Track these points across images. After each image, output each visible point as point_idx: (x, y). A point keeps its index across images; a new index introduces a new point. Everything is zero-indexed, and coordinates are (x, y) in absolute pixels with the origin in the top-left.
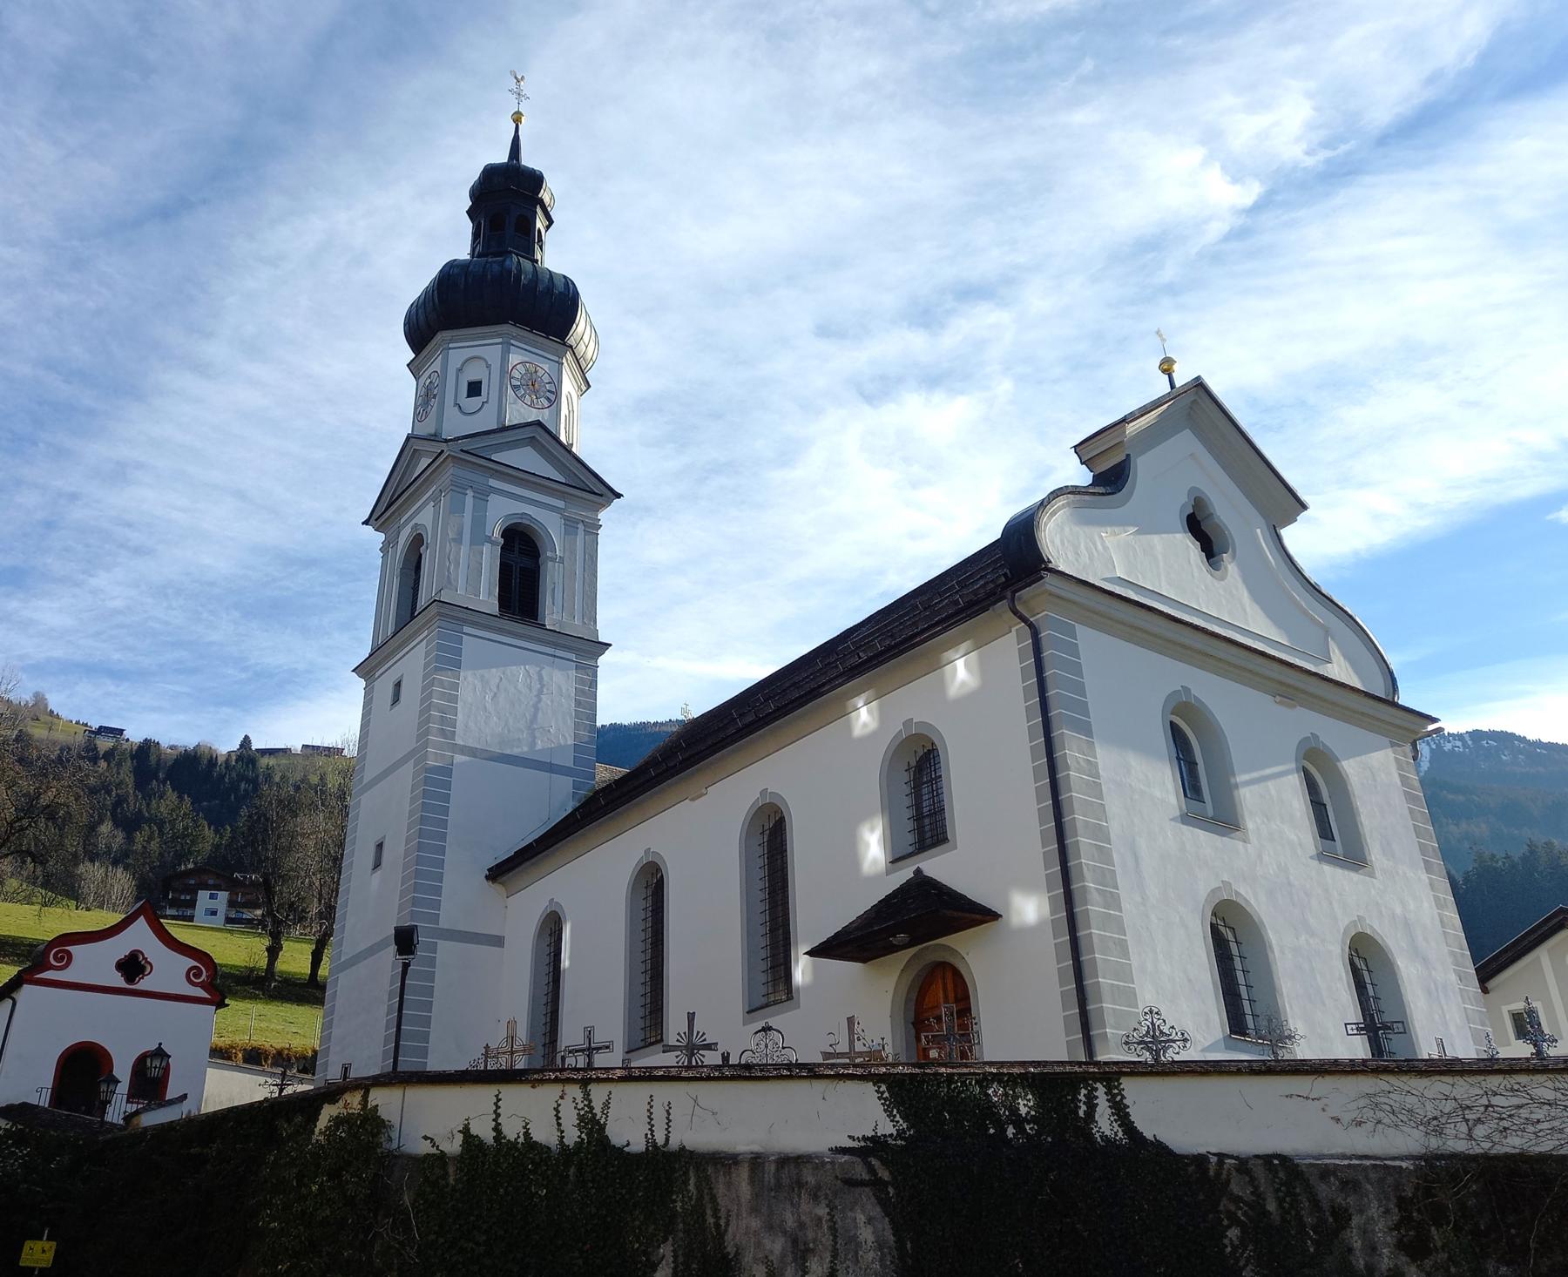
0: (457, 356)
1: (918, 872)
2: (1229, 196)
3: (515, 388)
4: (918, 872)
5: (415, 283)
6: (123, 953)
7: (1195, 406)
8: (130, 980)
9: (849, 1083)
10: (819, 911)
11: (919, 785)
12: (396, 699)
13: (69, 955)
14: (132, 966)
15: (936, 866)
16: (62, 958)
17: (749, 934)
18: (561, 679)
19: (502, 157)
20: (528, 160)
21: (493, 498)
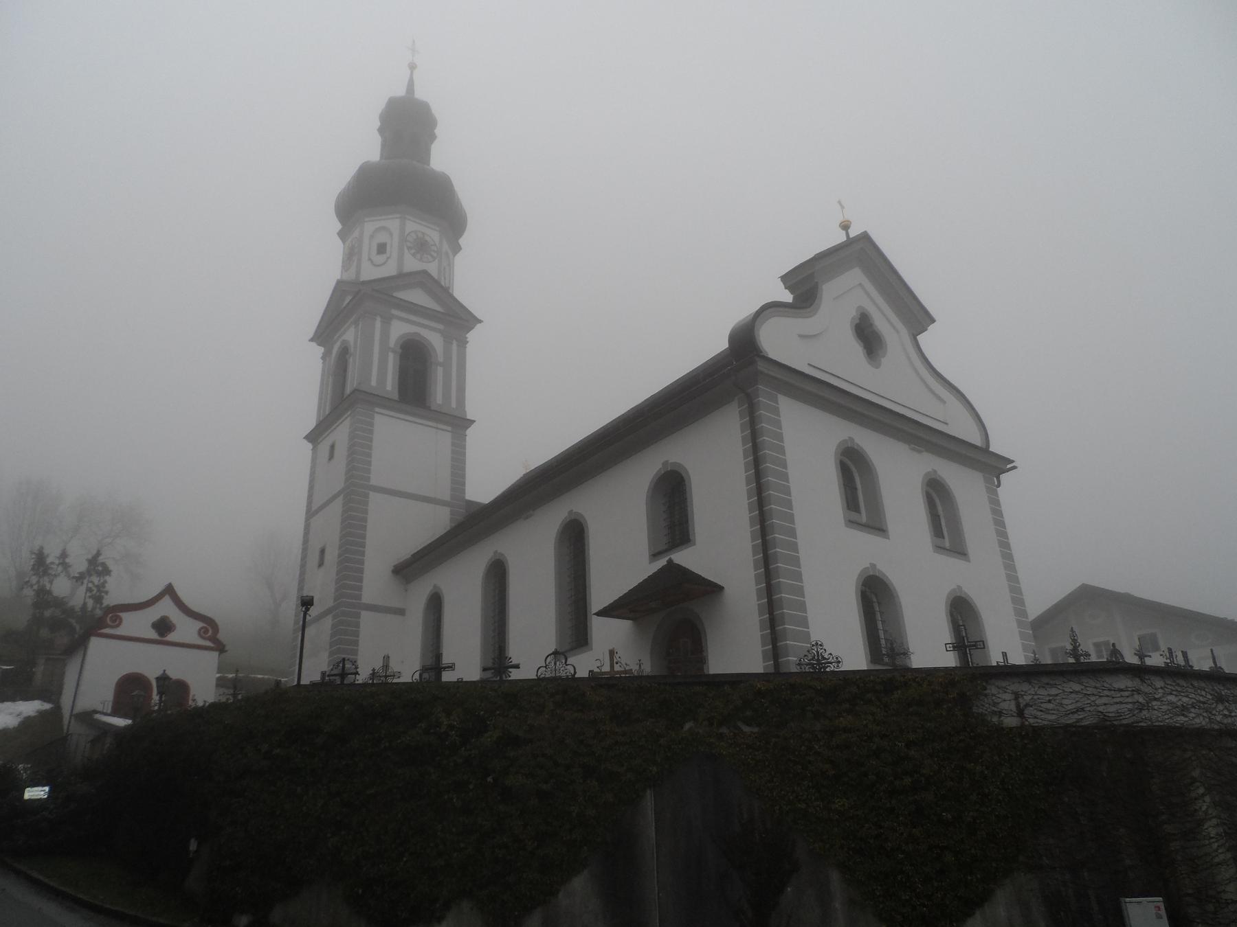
0: (369, 227)
1: (670, 561)
2: (1206, 666)
3: (409, 248)
4: (670, 561)
5: (341, 176)
7: (860, 253)
8: (162, 634)
10: (603, 591)
12: (331, 457)
13: (121, 620)
14: (163, 626)
15: (683, 558)
18: (442, 438)
19: (400, 92)
20: (420, 94)
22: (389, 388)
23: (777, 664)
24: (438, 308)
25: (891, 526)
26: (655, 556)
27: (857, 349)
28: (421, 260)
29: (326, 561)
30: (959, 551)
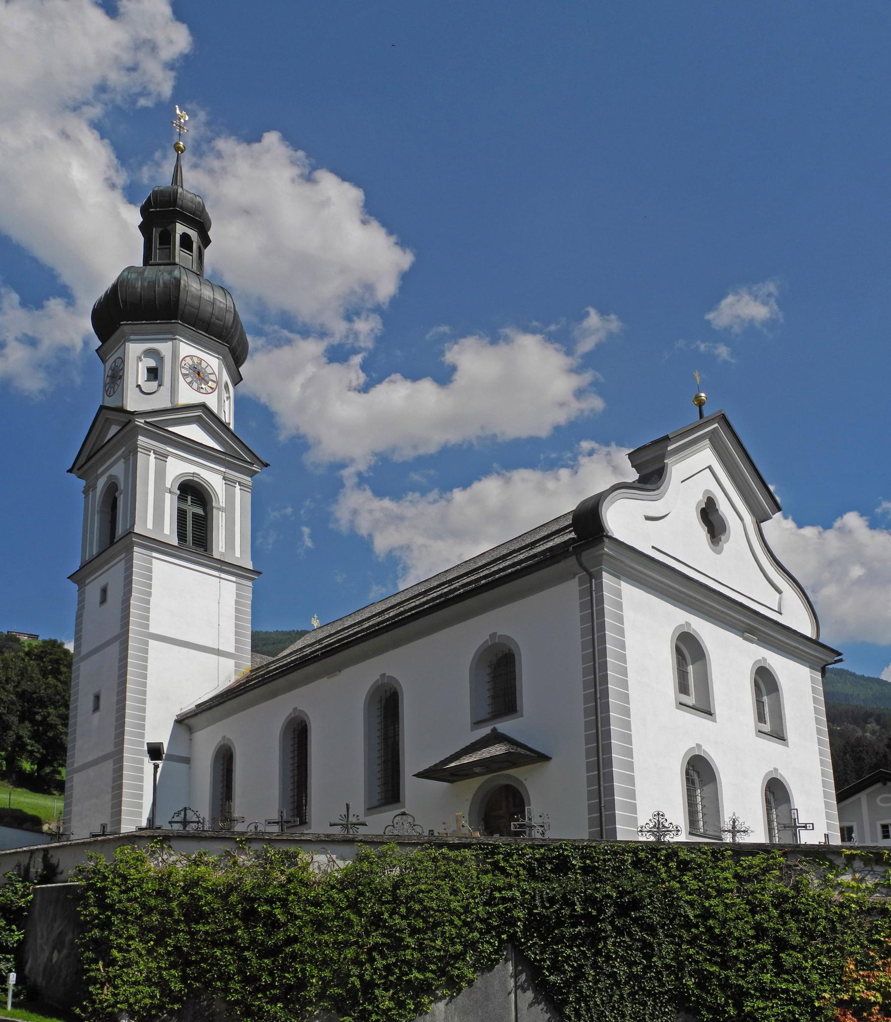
0: (134, 349)
1: (494, 730)
4: (494, 730)
11: (500, 680)
12: (103, 600)
21: (170, 459)
22: (167, 531)
23: (277, 823)
25: (719, 708)
26: (477, 723)
27: (701, 532)
28: (198, 390)
29: (101, 707)
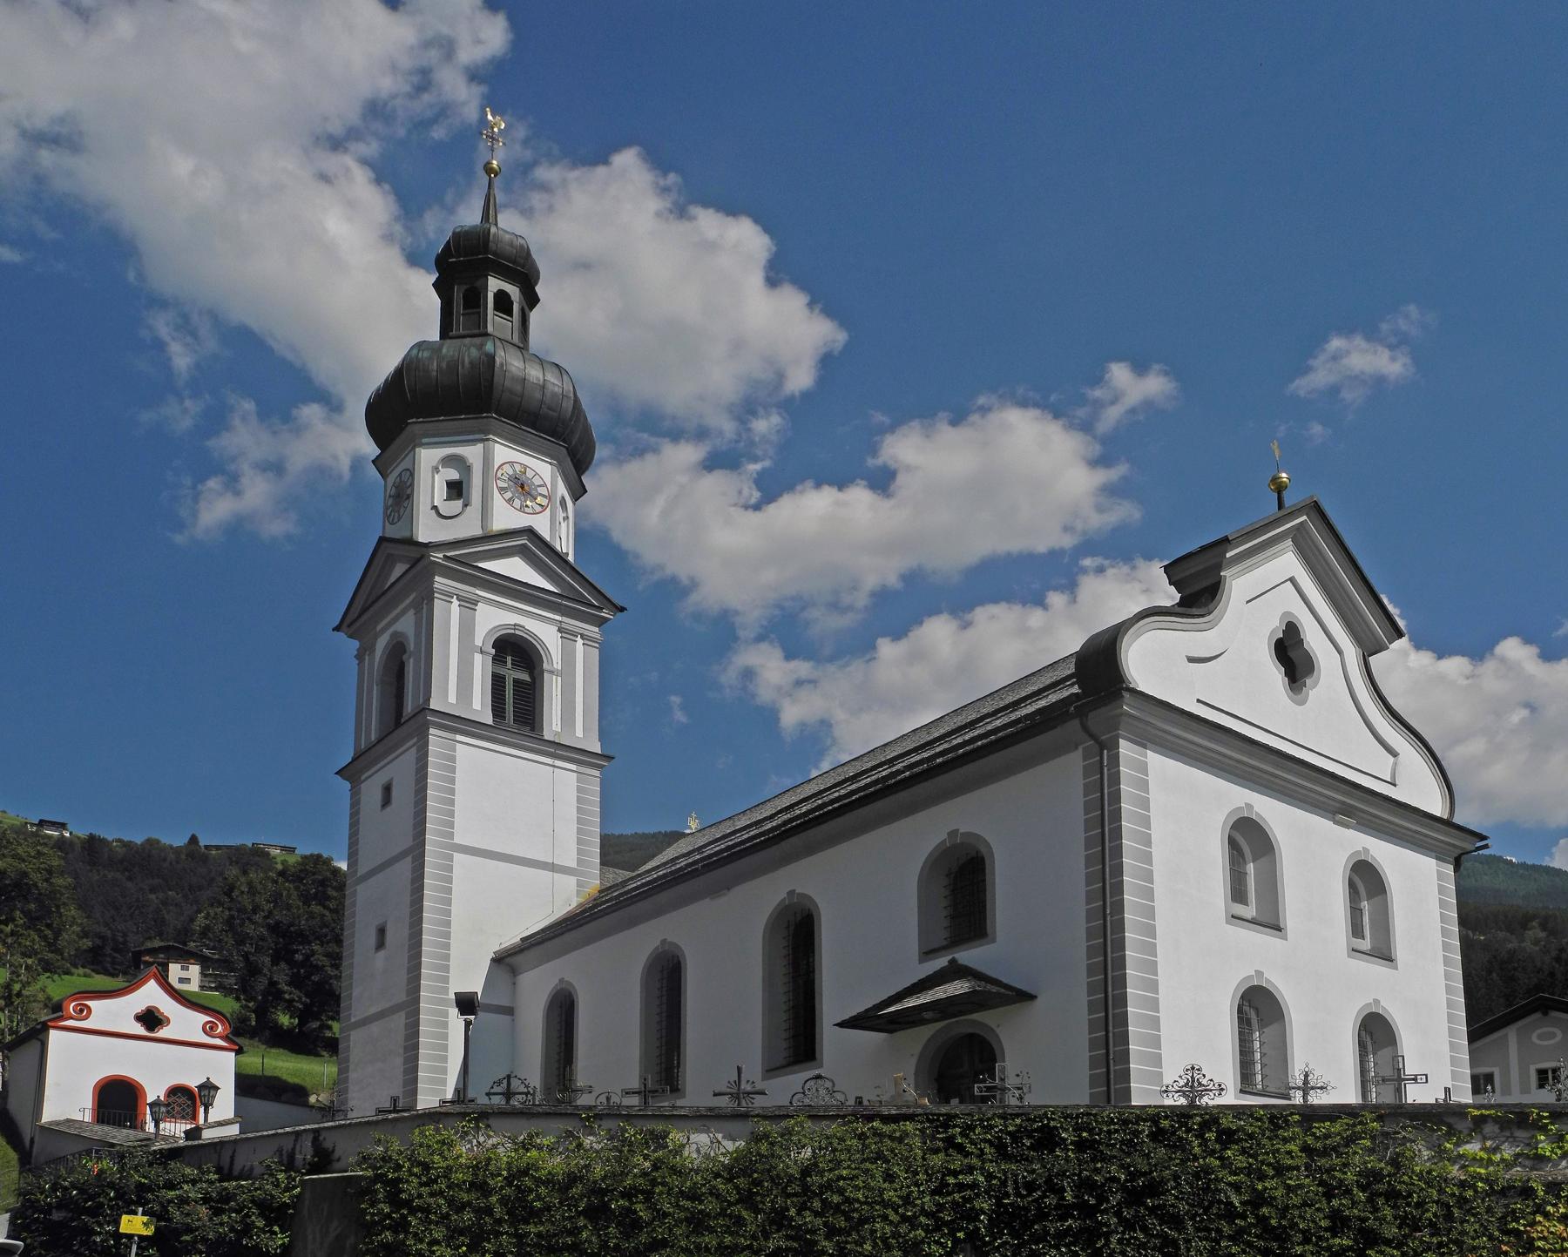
3: (501, 489)
6: (140, 1008)
8: (150, 1028)
9: (1005, 981)
10: (838, 998)
11: (962, 889)
13: (89, 1008)
16: (81, 1011)
17: (769, 1010)
24: (552, 588)
26: (927, 954)
27: (1275, 674)
28: (522, 509)
30: (1383, 954)
